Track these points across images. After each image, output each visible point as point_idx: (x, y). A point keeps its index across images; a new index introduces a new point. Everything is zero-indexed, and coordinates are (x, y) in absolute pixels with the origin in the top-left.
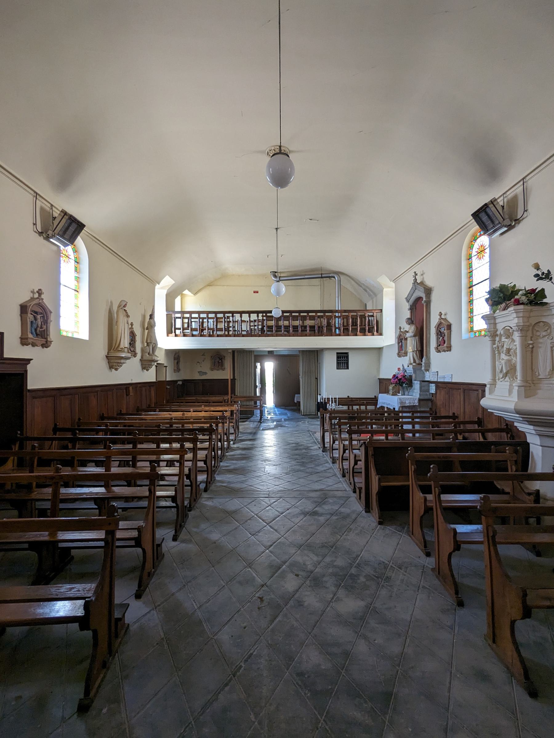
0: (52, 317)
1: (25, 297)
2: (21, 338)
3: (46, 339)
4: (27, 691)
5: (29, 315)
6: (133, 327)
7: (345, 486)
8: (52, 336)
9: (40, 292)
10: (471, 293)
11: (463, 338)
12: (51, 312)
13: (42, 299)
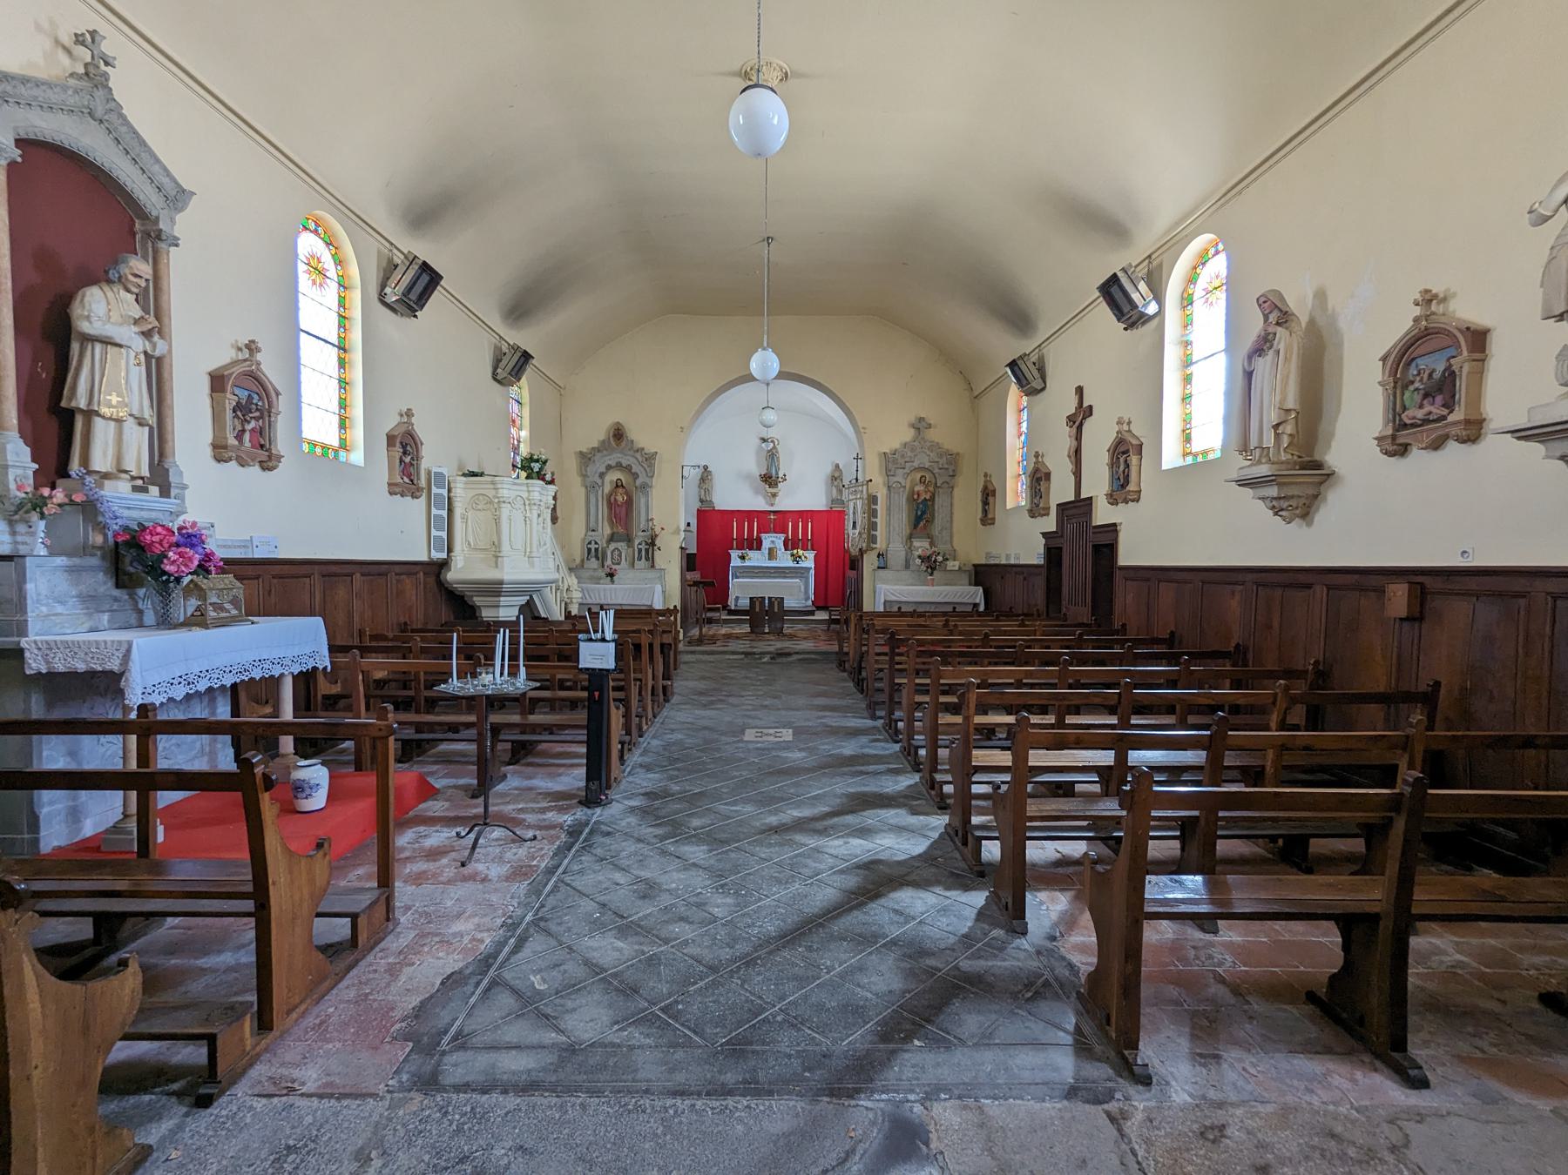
0: (282, 404)
1: (222, 356)
2: (215, 446)
3: (269, 450)
4: (1395, 514)
5: (229, 395)
6: (414, 420)
7: (397, 1026)
8: (282, 444)
9: (252, 347)
10: (1187, 380)
11: (1165, 467)
12: (278, 394)
13: (259, 364)
